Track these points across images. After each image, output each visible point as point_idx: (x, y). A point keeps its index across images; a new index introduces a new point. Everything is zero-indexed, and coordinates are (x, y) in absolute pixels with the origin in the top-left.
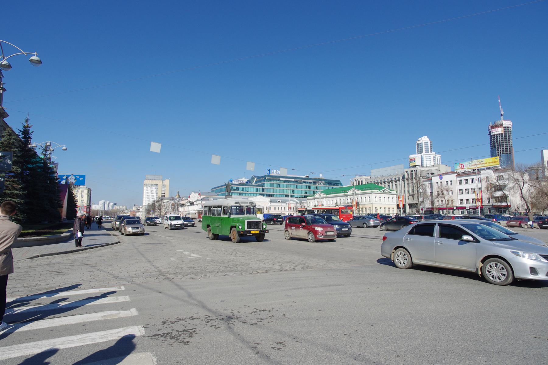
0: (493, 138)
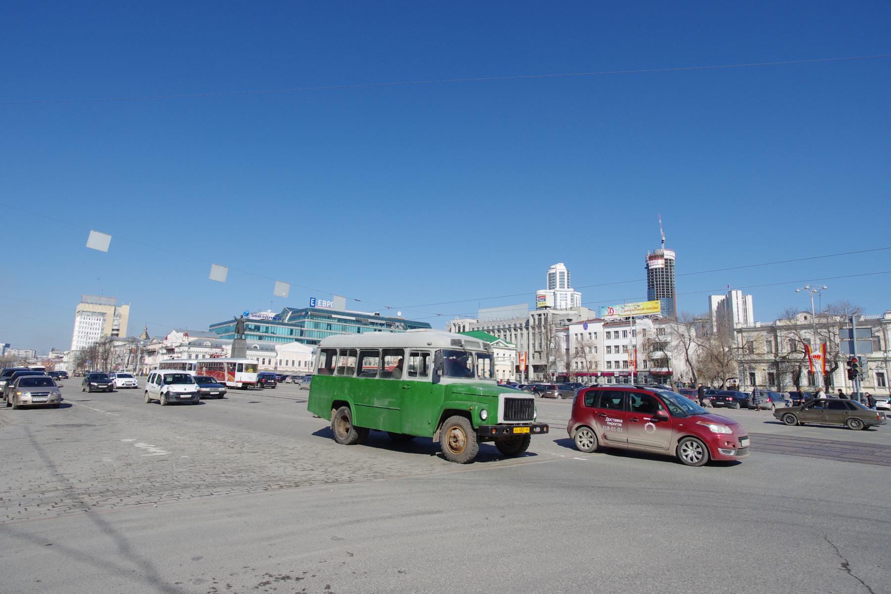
0: (651, 273)
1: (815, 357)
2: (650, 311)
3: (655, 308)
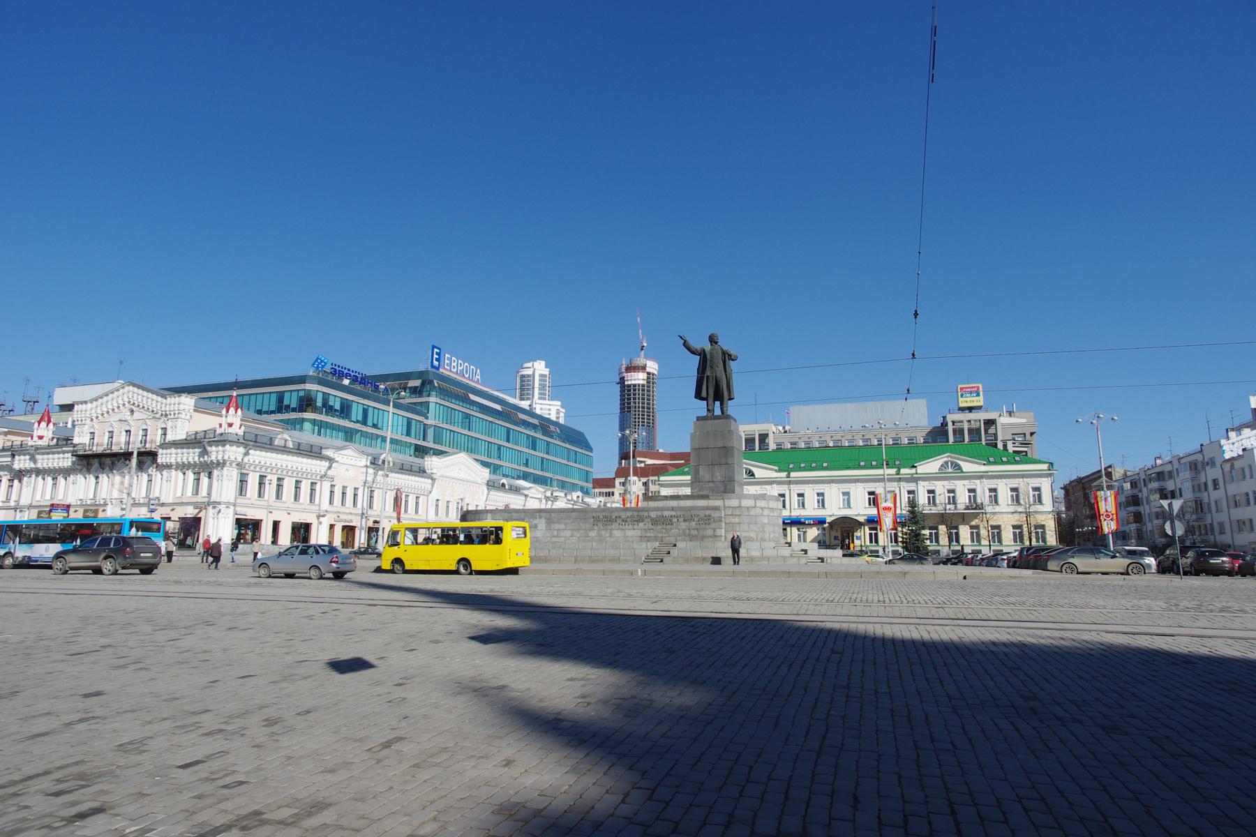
0: (626, 391)
1: (885, 509)
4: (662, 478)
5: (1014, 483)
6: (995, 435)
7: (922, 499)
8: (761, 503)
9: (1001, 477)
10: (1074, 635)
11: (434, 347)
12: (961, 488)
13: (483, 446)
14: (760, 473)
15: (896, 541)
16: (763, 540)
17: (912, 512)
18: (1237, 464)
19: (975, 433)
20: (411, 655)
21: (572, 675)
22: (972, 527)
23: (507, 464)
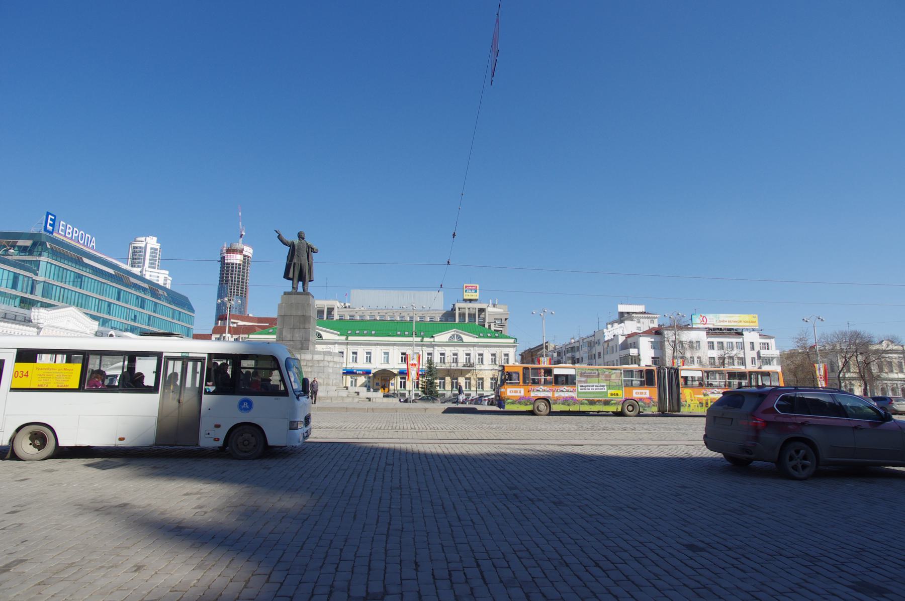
0: (225, 268)
1: (412, 365)
2: (733, 324)
3: (752, 322)
4: (251, 336)
5: (494, 350)
6: (484, 319)
7: (436, 359)
8: (328, 358)
9: (361, 344)
10: (532, 447)
11: (48, 214)
12: (462, 352)
13: (93, 302)
14: (326, 336)
15: (418, 387)
16: (328, 384)
17: (430, 368)
18: (611, 344)
19: (472, 316)
20: (23, 485)
21: (188, 491)
22: (466, 379)
23: (116, 319)
